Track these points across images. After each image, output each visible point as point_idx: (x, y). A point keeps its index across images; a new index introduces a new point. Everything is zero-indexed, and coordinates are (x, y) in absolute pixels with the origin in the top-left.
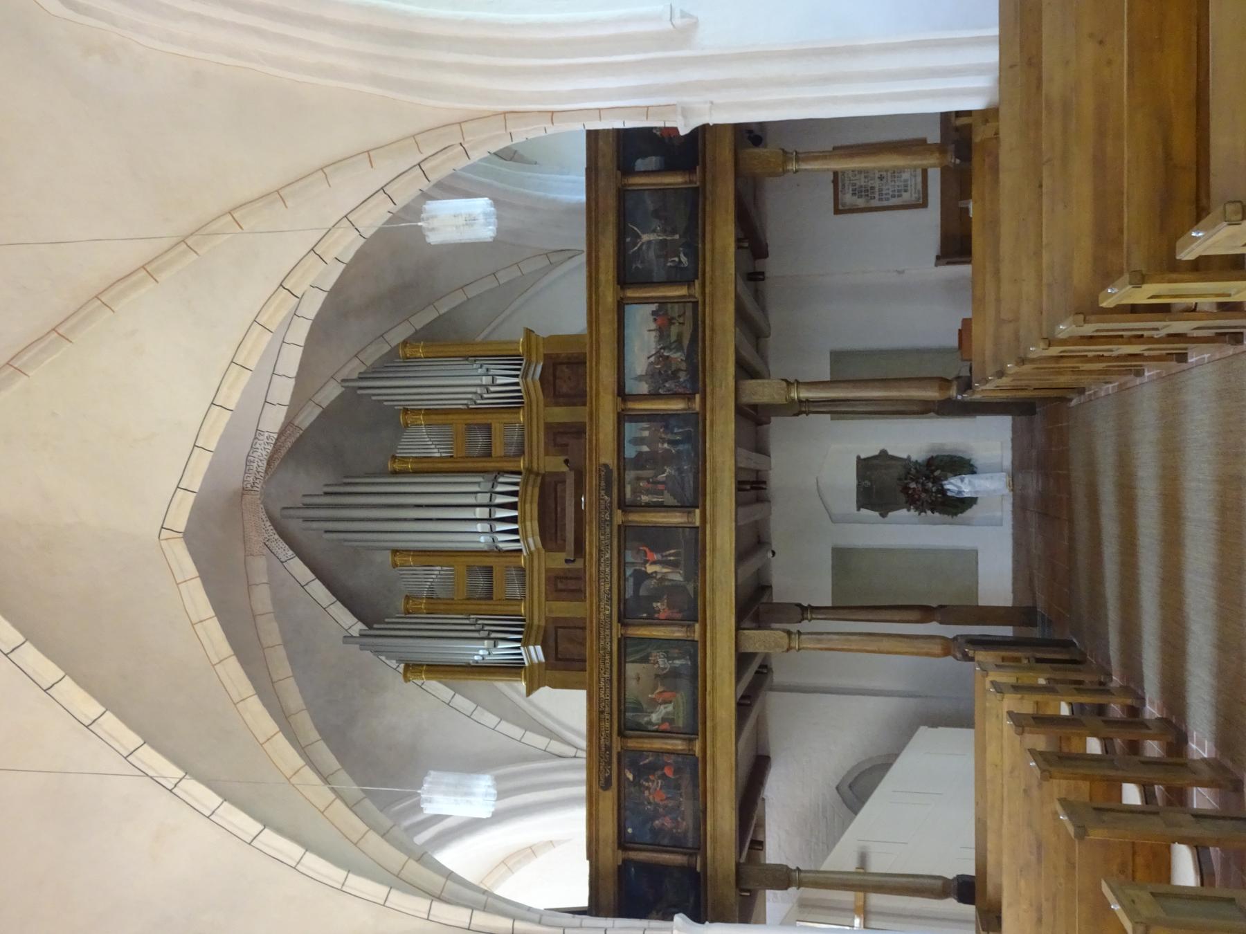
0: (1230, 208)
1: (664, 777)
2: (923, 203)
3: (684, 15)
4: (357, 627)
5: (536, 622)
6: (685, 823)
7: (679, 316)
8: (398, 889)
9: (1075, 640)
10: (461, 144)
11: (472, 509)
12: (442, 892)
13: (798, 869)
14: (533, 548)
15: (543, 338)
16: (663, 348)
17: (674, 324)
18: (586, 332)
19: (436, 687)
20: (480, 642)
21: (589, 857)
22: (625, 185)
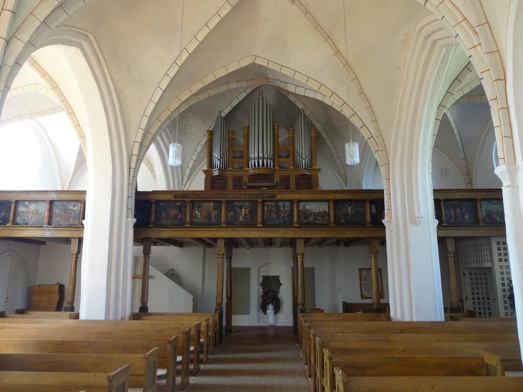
0: (346, 379)
1: (178, 215)
2: (363, 297)
3: (420, 221)
4: (224, 115)
5: (226, 173)
6: (163, 221)
7: (324, 219)
8: (144, 132)
9: (222, 345)
10: (379, 150)
11: (262, 152)
12: (143, 146)
13: (150, 257)
14: (249, 172)
15: (317, 175)
16: (314, 214)
17: (322, 218)
18: (320, 189)
19: (205, 139)
20: (219, 155)
21: (153, 191)
22: (366, 202)
